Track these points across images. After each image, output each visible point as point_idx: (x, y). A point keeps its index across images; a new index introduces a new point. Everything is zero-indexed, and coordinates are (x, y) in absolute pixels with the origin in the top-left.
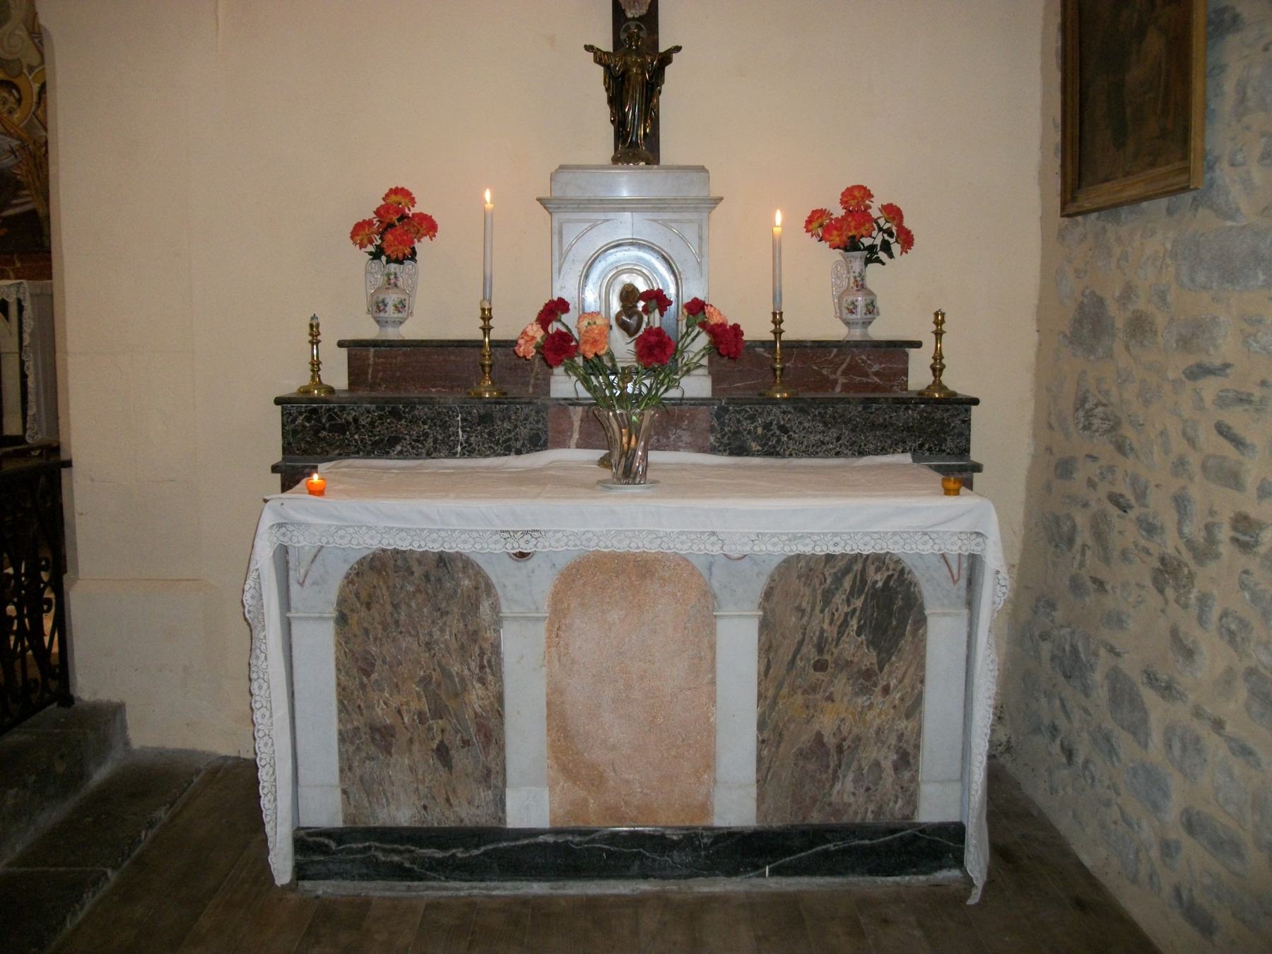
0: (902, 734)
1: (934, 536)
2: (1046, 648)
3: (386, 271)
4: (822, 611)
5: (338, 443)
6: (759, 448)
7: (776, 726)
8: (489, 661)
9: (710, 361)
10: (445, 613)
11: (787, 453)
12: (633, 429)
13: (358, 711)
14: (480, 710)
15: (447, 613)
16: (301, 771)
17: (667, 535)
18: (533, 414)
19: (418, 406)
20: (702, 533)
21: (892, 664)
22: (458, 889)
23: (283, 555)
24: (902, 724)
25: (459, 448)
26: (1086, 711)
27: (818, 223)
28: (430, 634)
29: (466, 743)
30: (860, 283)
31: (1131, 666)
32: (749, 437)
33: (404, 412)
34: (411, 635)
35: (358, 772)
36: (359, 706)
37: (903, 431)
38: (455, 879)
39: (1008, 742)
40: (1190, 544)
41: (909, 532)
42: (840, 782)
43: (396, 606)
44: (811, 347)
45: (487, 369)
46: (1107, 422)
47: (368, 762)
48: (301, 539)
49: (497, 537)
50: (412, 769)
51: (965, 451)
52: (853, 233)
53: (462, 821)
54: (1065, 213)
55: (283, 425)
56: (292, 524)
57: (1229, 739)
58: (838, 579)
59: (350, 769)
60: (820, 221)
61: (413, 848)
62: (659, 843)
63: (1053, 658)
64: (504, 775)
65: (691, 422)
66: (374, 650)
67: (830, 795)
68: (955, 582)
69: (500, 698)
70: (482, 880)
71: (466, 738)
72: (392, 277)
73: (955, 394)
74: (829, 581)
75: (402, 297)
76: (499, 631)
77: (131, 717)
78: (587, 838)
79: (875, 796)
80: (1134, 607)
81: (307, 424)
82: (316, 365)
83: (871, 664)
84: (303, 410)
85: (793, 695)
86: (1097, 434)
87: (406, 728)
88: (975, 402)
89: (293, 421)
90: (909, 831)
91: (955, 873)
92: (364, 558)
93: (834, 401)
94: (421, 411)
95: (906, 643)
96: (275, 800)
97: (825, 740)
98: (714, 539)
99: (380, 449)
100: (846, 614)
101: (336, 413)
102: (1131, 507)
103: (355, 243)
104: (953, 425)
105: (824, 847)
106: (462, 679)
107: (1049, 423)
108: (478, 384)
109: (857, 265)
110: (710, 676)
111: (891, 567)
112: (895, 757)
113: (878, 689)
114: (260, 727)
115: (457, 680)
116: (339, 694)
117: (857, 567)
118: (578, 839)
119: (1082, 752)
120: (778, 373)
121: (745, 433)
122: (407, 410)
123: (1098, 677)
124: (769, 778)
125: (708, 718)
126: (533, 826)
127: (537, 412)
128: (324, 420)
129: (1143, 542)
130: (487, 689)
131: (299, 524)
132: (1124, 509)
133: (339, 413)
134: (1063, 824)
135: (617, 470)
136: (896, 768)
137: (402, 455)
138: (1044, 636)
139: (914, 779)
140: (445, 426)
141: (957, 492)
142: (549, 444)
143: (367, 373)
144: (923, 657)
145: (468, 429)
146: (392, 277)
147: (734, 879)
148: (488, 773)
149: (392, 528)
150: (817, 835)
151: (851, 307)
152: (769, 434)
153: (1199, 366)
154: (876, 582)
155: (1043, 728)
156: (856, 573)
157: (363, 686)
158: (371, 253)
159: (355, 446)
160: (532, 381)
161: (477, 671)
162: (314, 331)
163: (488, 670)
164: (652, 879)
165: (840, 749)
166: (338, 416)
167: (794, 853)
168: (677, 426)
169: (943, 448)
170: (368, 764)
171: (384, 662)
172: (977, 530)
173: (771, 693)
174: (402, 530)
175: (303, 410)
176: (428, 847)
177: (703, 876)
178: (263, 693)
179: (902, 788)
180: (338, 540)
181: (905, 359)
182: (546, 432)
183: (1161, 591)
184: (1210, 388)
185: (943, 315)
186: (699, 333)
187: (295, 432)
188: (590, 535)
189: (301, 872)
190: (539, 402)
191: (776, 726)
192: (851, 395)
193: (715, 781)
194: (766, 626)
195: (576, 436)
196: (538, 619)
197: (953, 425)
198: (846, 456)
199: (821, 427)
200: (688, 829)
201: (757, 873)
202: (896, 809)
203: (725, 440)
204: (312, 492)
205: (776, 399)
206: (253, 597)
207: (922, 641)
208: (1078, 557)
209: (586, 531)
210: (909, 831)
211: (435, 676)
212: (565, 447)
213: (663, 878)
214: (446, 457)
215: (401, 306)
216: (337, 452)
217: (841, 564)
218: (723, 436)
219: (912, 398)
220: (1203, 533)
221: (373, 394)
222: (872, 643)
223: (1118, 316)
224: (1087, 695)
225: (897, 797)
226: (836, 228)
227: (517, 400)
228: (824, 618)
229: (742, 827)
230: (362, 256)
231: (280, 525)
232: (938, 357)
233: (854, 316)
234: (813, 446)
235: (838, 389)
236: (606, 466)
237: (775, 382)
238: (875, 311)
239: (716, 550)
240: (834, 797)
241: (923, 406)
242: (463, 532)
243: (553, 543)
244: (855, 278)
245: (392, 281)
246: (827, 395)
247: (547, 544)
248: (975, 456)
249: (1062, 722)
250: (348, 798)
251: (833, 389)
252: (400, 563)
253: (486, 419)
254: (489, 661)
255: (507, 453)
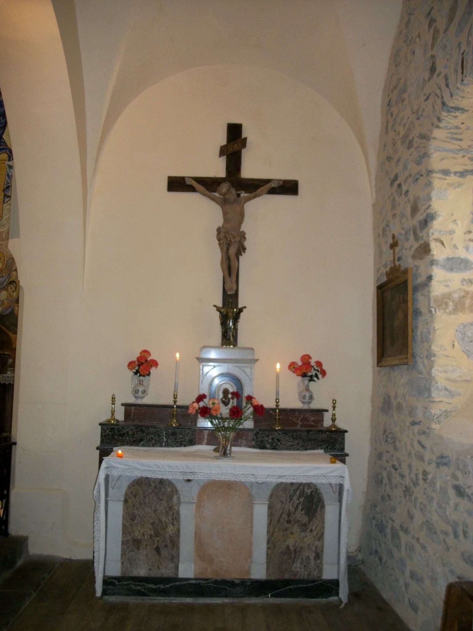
0: (317, 547)
1: (327, 477)
2: (374, 522)
3: (139, 379)
4: (289, 502)
5: (121, 440)
6: (270, 447)
7: (273, 543)
8: (176, 517)
9: (254, 417)
10: (161, 500)
11: (280, 449)
12: (227, 439)
13: (129, 533)
14: (171, 534)
15: (162, 500)
16: (107, 554)
17: (238, 475)
18: (191, 432)
19: (150, 428)
20: (249, 474)
21: (313, 521)
22: (160, 600)
23: (107, 478)
24: (317, 543)
25: (164, 444)
26: (386, 543)
27: (293, 367)
28: (156, 507)
29: (166, 546)
30: (307, 388)
31: (397, 525)
32: (266, 442)
33: (145, 430)
34: (149, 507)
35: (127, 556)
36: (130, 532)
37: (321, 442)
38: (159, 596)
39: (363, 560)
40: (412, 480)
41: (318, 476)
42: (295, 563)
43: (145, 497)
44: (289, 411)
45: (175, 416)
46: (392, 439)
47: (131, 552)
48: (115, 472)
49: (181, 474)
50: (147, 555)
51: (343, 449)
52: (304, 371)
53: (163, 574)
54: (378, 366)
55: (101, 433)
56: (111, 467)
57: (420, 544)
58: (295, 492)
59: (125, 555)
60: (293, 366)
61: (145, 584)
62: (231, 584)
63: (376, 525)
64: (179, 558)
65: (246, 436)
66: (136, 512)
67: (292, 568)
68: (335, 493)
69: (179, 530)
70: (169, 597)
71: (166, 544)
72: (141, 381)
73: (339, 429)
74: (292, 492)
75: (145, 389)
76: (179, 507)
77: (30, 542)
78: (207, 582)
79: (307, 569)
80: (399, 504)
81: (110, 433)
82: (113, 413)
83: (306, 521)
84: (109, 428)
85: (279, 532)
86: (389, 444)
87: (145, 540)
88: (346, 431)
89: (105, 432)
90: (319, 582)
91: (336, 598)
92: (135, 480)
93: (296, 431)
94: (151, 430)
95: (318, 515)
96: (99, 564)
97: (290, 548)
98: (253, 476)
99: (136, 443)
100: (298, 504)
101: (121, 430)
102: (398, 469)
103: (129, 369)
104: (338, 440)
105: (290, 587)
106: (166, 523)
107: (375, 439)
108: (171, 421)
109: (306, 382)
110: (251, 524)
111: (313, 487)
112: (315, 555)
113: (308, 530)
114: (96, 537)
115: (164, 523)
116: (123, 527)
117: (301, 487)
118: (204, 582)
119: (384, 558)
120: (277, 420)
121: (265, 441)
122: (146, 429)
123: (388, 531)
124: (271, 561)
125: (250, 539)
126: (188, 577)
127: (192, 432)
128: (116, 432)
129: (401, 481)
130: (174, 527)
131: (114, 467)
132: (396, 470)
133: (122, 430)
134: (379, 586)
135: (221, 452)
136: (315, 559)
137: (143, 445)
138: (374, 519)
139: (321, 563)
140: (159, 436)
141: (335, 462)
142: (196, 443)
143: (131, 415)
144: (324, 519)
145: (167, 437)
146: (141, 381)
147: (258, 598)
148: (172, 558)
149: (145, 470)
150: (287, 582)
151: (304, 397)
152: (274, 442)
153: (414, 421)
154: (307, 493)
155: (373, 552)
156: (301, 490)
157: (131, 525)
158: (134, 372)
159: (127, 442)
160: (190, 421)
161: (171, 521)
162: (113, 399)
163: (175, 520)
164: (229, 598)
165: (295, 552)
166: (121, 431)
167: (279, 589)
168: (241, 438)
169: (335, 448)
170: (131, 553)
171: (139, 516)
172: (342, 475)
173: (271, 531)
174: (148, 470)
175: (109, 428)
176: (150, 584)
177: (247, 596)
178: (98, 525)
179: (317, 566)
180: (127, 473)
181: (322, 416)
182: (195, 439)
183: (405, 497)
184: (416, 428)
185: (335, 401)
186: (250, 407)
187: (105, 436)
188: (212, 474)
189: (104, 593)
190: (193, 428)
191: (273, 543)
192: (303, 428)
193: (252, 562)
194: (270, 507)
195: (205, 441)
196: (193, 503)
197: (338, 440)
198: (301, 450)
199: (292, 440)
200: (242, 579)
201: (266, 596)
202: (315, 574)
203: (258, 444)
204: (118, 456)
205: (276, 429)
206: (97, 492)
207: (323, 514)
208: (384, 488)
209: (211, 473)
210: (319, 582)
211: (157, 522)
212: (202, 445)
213: (233, 597)
214: (159, 447)
215: (144, 392)
216: (120, 443)
217: (296, 486)
218: (257, 442)
219: (324, 430)
220: (415, 477)
221: (134, 423)
222: (306, 514)
223: (394, 403)
224: (386, 537)
225: (315, 569)
226: (299, 369)
227: (186, 427)
228: (290, 504)
229: (261, 579)
230: (131, 373)
231: (107, 468)
232: (334, 415)
233: (305, 400)
234: (289, 446)
235: (299, 426)
236: (216, 452)
237: (276, 423)
238: (313, 398)
239: (254, 480)
240: (293, 569)
241: (328, 433)
242: (170, 472)
243: (200, 477)
244: (306, 386)
245: (141, 383)
246: (294, 428)
247: (197, 477)
248: (347, 451)
249: (379, 550)
250: (123, 565)
251: (297, 426)
252: (147, 482)
253: (174, 434)
254: (176, 517)
255: (181, 446)
